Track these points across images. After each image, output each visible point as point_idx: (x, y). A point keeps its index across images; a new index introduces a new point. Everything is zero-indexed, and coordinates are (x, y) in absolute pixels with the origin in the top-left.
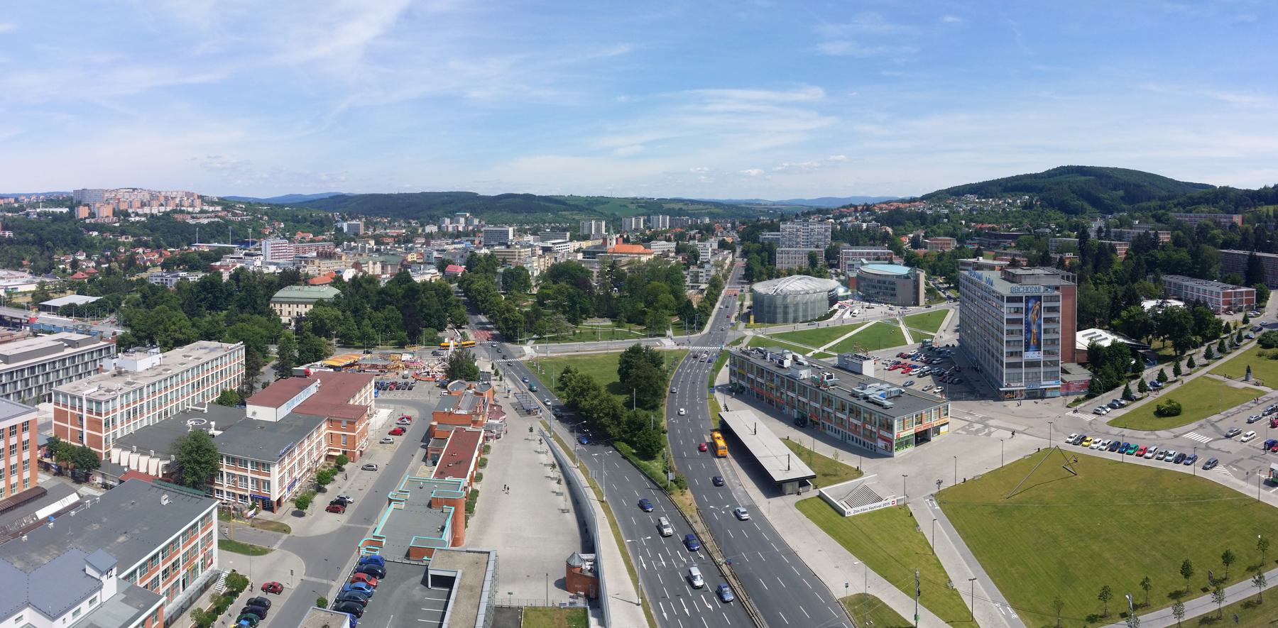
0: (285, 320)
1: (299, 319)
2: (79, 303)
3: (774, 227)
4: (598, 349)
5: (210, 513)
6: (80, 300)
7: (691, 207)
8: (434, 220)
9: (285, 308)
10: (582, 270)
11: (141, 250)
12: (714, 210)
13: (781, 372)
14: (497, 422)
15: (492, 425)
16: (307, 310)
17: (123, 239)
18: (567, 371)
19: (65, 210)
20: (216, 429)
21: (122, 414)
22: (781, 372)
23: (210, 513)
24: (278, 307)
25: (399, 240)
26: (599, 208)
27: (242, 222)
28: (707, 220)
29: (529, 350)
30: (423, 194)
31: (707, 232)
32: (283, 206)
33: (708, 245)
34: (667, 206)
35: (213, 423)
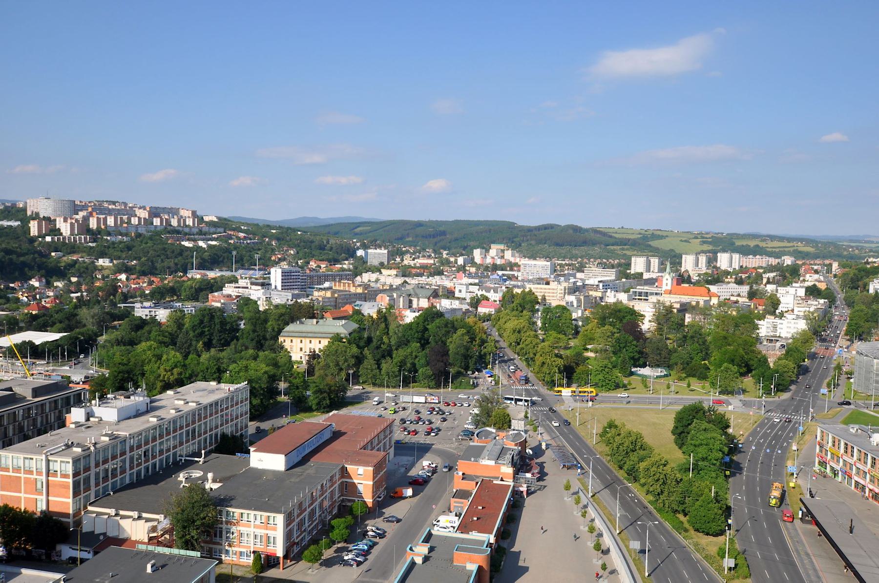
0: (295, 357)
1: (313, 356)
2: (37, 342)
6: (39, 338)
7: (771, 244)
8: (467, 250)
9: (296, 341)
10: (156, 234)
11: (123, 277)
16: (321, 346)
17: (101, 262)
18: (611, 425)
19: (15, 224)
20: (214, 481)
21: (97, 474)
24: (288, 340)
26: (655, 243)
27: (247, 246)
30: (456, 222)
31: (787, 276)
32: (295, 230)
34: (738, 243)
35: (210, 476)
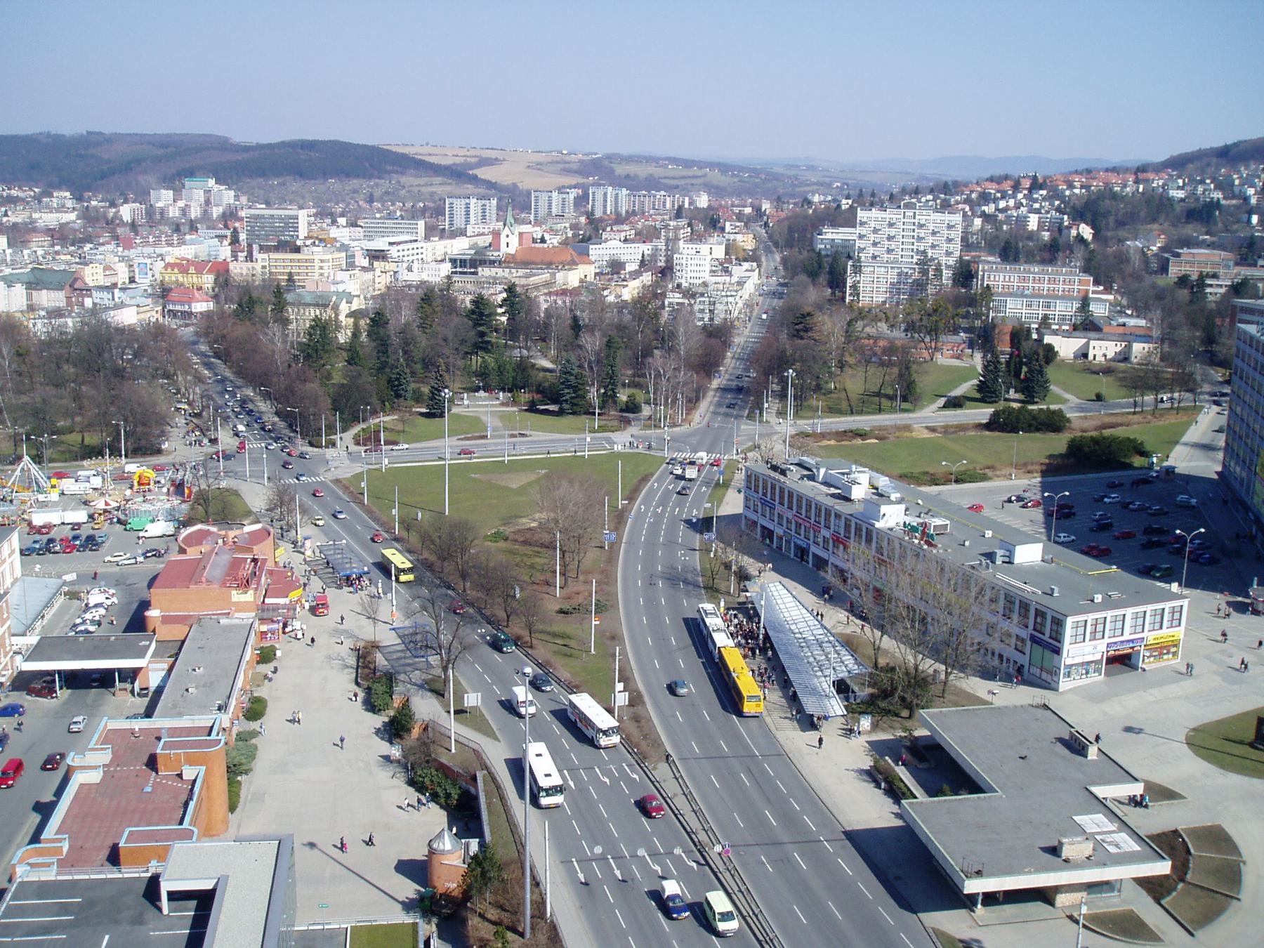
3: (849, 220)
4: (487, 439)
5: (928, 714)
12: (715, 176)
13: (841, 507)
14: (282, 601)
15: (276, 608)
22: (841, 507)
23: (928, 714)
25: (60, 235)
28: (703, 201)
29: (341, 458)
33: (704, 248)
34: (620, 170)
